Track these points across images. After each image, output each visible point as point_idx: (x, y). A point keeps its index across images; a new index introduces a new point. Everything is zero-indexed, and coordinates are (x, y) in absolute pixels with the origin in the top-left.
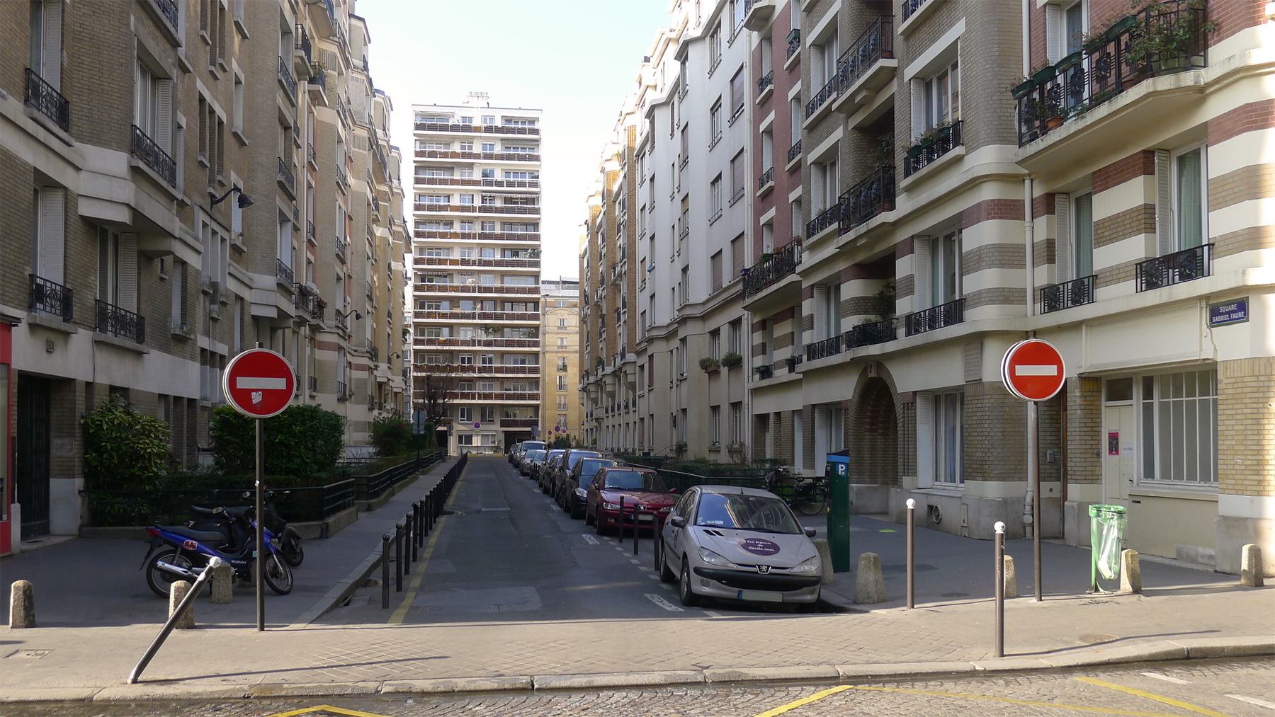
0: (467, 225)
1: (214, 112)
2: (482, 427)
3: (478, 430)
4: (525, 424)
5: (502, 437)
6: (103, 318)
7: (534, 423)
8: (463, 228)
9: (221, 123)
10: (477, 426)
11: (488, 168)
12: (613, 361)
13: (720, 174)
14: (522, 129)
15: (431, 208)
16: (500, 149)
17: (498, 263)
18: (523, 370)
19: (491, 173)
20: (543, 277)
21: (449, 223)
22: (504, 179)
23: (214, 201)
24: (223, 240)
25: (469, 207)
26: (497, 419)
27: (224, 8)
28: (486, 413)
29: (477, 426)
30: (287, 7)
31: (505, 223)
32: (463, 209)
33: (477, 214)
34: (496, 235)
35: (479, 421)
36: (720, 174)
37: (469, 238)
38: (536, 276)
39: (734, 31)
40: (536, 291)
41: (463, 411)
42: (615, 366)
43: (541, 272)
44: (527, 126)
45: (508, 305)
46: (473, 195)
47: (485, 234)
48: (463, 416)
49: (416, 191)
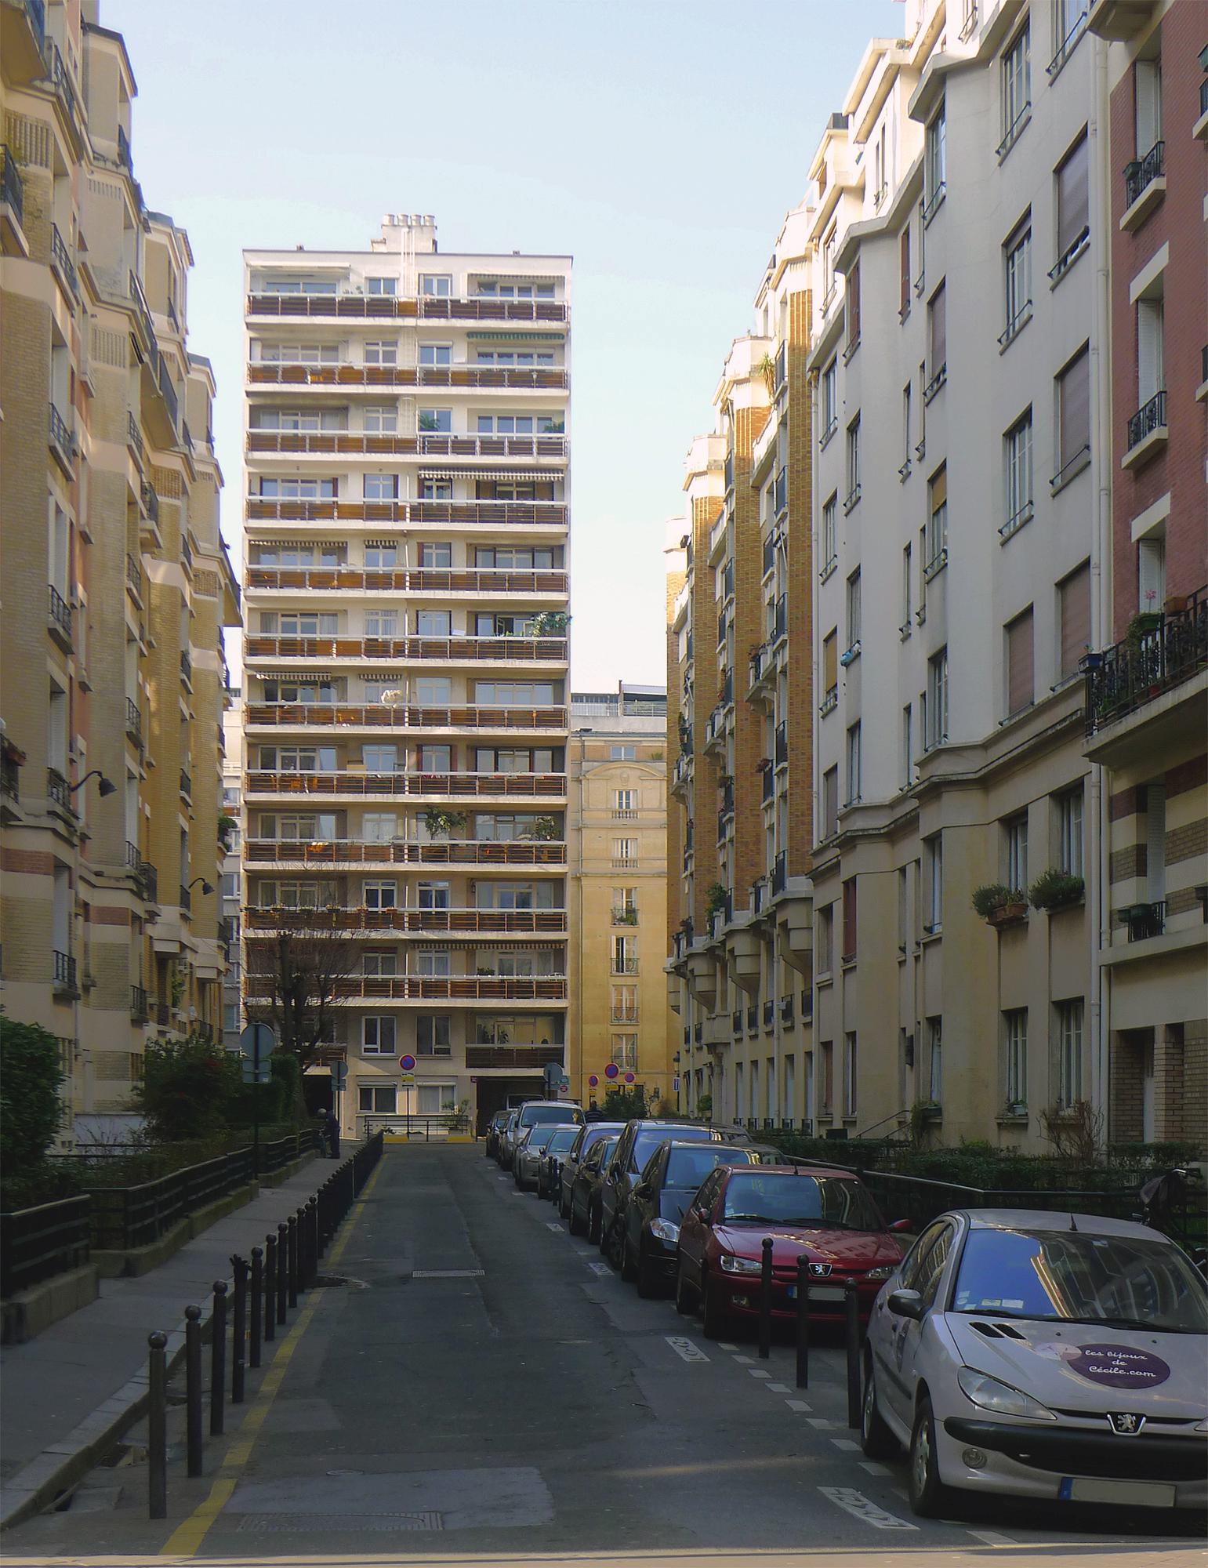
2: (420, 1067)
3: (408, 1075)
5: (470, 1092)
10: (407, 1064)
11: (435, 409)
15: (291, 511)
18: (523, 922)
19: (444, 421)
20: (578, 684)
22: (476, 435)
31: (478, 548)
33: (407, 525)
35: (412, 1052)
44: (534, 299)
46: (396, 477)
48: (371, 1039)
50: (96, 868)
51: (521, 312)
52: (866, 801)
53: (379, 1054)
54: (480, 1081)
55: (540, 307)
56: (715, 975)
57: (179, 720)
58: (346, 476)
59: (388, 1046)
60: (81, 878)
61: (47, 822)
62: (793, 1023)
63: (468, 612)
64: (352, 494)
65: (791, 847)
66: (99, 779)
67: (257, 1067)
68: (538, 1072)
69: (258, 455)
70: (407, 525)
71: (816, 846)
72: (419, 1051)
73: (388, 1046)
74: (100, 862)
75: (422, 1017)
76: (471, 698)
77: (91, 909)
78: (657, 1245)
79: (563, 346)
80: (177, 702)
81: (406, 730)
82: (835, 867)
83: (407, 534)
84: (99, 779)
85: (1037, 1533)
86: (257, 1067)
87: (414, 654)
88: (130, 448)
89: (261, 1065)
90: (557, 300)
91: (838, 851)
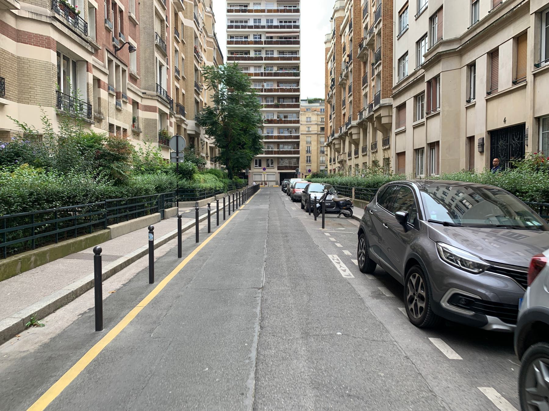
0: (258, 53)
1: (116, 4)
2: (267, 170)
3: (264, 172)
4: (291, 168)
5: (278, 176)
6: (71, 203)
7: (296, 168)
8: (256, 54)
9: (121, 11)
10: (264, 169)
11: (270, 18)
12: (339, 130)
13: (407, 52)
14: (289, 10)
15: (237, 43)
16: (276, 70)
17: (276, 74)
18: (290, 137)
19: (272, 21)
20: (302, 98)
21: (248, 52)
22: (279, 24)
23: (117, 49)
24: (124, 71)
25: (259, 41)
26: (276, 165)
27: (122, 11)
28: (270, 162)
29: (264, 169)
30: (156, 4)
31: (280, 67)
32: (256, 43)
33: (263, 46)
34: (274, 58)
35: (266, 167)
36: (407, 52)
37: (259, 76)
38: (297, 98)
39: (420, 11)
40: (298, 106)
41: (256, 161)
42: (341, 132)
43: (301, 80)
44: (292, 24)
45: (281, 146)
46: (261, 35)
47: (268, 57)
48: (256, 164)
49: (229, 34)
50: (144, 91)
51: (290, 27)
52: (445, 38)
53: (258, 167)
54: (281, 173)
55: (294, 26)
56: (359, 133)
57: (194, 71)
58: (249, 35)
59: (260, 165)
60: (128, 89)
61: (157, 98)
62: (390, 146)
63: (278, 51)
64: (251, 38)
65: (383, 89)
66: (129, 45)
67: (177, 155)
68: (294, 171)
69: (229, 30)
70: (263, 46)
71: (393, 86)
72: (267, 166)
73: (260, 165)
74: (145, 89)
75: (267, 159)
76: (278, 86)
77: (139, 105)
78: (244, 169)
79: (299, 4)
80: (193, 61)
81: (264, 93)
82: (423, 77)
83: (263, 48)
84: (129, 45)
85: (69, 41)
86: (177, 155)
87: (265, 76)
88: (194, 21)
89: (179, 155)
90: (297, 24)
91: (424, 70)
